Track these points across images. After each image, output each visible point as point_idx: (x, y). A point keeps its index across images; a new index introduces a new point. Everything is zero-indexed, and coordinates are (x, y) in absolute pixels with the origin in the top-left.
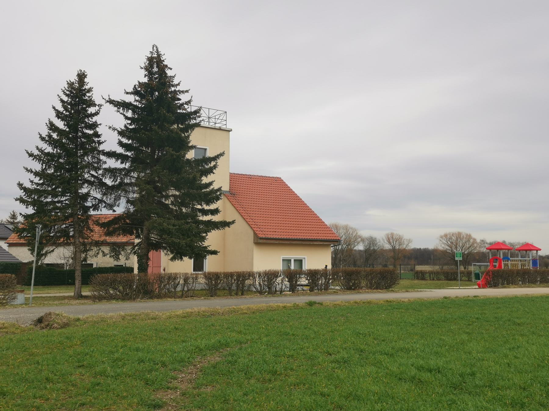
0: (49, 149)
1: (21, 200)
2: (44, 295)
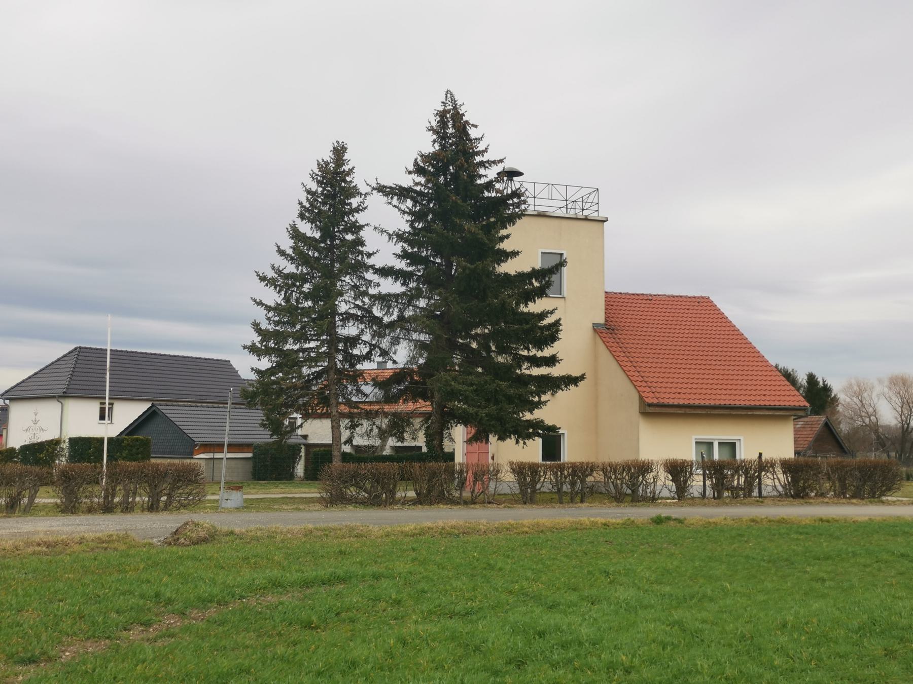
0: (290, 268)
1: (253, 349)
2: (297, 496)
